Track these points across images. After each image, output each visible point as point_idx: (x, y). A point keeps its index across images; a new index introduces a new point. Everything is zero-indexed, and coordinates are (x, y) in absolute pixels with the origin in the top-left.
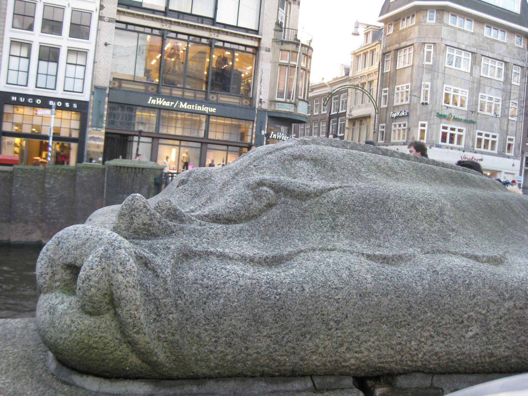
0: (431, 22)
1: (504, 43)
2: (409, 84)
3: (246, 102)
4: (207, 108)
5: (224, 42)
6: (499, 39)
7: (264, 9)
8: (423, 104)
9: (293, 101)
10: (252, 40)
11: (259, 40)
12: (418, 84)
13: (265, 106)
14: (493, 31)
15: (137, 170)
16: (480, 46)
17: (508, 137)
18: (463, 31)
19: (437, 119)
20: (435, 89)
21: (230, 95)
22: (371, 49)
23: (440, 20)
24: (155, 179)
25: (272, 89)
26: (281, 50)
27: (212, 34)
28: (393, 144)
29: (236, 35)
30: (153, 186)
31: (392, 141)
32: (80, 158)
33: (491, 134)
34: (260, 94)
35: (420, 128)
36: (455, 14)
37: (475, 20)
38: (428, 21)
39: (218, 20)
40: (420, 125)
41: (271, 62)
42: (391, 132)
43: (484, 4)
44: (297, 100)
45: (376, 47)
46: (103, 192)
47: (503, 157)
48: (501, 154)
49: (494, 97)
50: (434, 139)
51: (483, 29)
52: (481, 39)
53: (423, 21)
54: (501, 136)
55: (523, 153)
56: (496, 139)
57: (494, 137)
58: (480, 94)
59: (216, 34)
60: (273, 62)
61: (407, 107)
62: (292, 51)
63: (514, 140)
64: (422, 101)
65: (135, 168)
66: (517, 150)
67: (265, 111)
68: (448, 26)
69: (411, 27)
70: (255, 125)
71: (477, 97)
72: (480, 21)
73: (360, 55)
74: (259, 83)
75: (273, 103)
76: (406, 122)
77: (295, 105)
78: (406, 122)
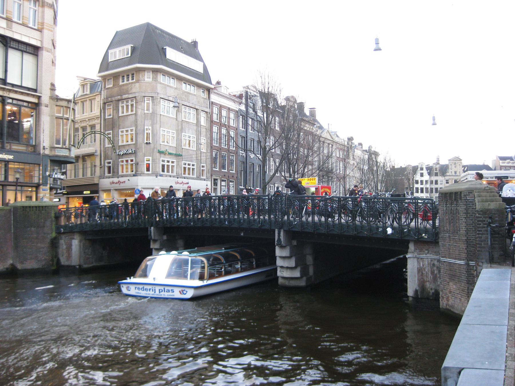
0: (148, 80)
1: (195, 95)
2: (134, 128)
3: (31, 149)
4: (7, 156)
5: (13, 99)
6: (192, 92)
7: (41, 72)
8: (147, 143)
9: (67, 147)
10: (34, 97)
11: (39, 97)
12: (142, 128)
13: (47, 152)
14: (188, 86)
15: (41, 208)
16: (181, 98)
17: (202, 165)
18: (170, 87)
19: (158, 154)
20: (155, 133)
21: (20, 144)
22: (90, 98)
23: (155, 79)
24: (55, 214)
25: (51, 137)
26: (57, 106)
27: (5, 92)
28: (122, 176)
29: (22, 93)
30: (54, 219)
31: (120, 173)
32: (37, 199)
33: (191, 163)
34: (43, 142)
35: (146, 162)
36: (164, 74)
37: (177, 79)
38: (146, 79)
39: (9, 81)
40: (145, 160)
41: (49, 116)
42: (118, 166)
43: (182, 66)
44: (71, 146)
45: (97, 97)
46: (11, 228)
47: (200, 180)
48: (198, 178)
49: (191, 136)
50: (158, 170)
51: (182, 85)
52: (181, 92)
53: (142, 79)
54: (197, 164)
55: (211, 176)
56: (195, 167)
57: (193, 165)
58: (183, 134)
59: (8, 93)
60: (51, 116)
61: (133, 146)
62: (65, 107)
63: (205, 167)
64: (146, 141)
65: (39, 207)
66: (208, 174)
67: (47, 156)
68: (161, 83)
69: (132, 83)
70: (41, 168)
71: (181, 135)
72: (180, 79)
73: (78, 102)
74: (42, 133)
75: (53, 149)
76: (134, 159)
77: (69, 149)
78: (134, 159)
